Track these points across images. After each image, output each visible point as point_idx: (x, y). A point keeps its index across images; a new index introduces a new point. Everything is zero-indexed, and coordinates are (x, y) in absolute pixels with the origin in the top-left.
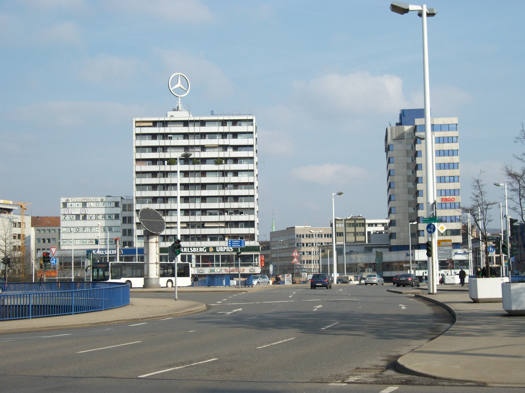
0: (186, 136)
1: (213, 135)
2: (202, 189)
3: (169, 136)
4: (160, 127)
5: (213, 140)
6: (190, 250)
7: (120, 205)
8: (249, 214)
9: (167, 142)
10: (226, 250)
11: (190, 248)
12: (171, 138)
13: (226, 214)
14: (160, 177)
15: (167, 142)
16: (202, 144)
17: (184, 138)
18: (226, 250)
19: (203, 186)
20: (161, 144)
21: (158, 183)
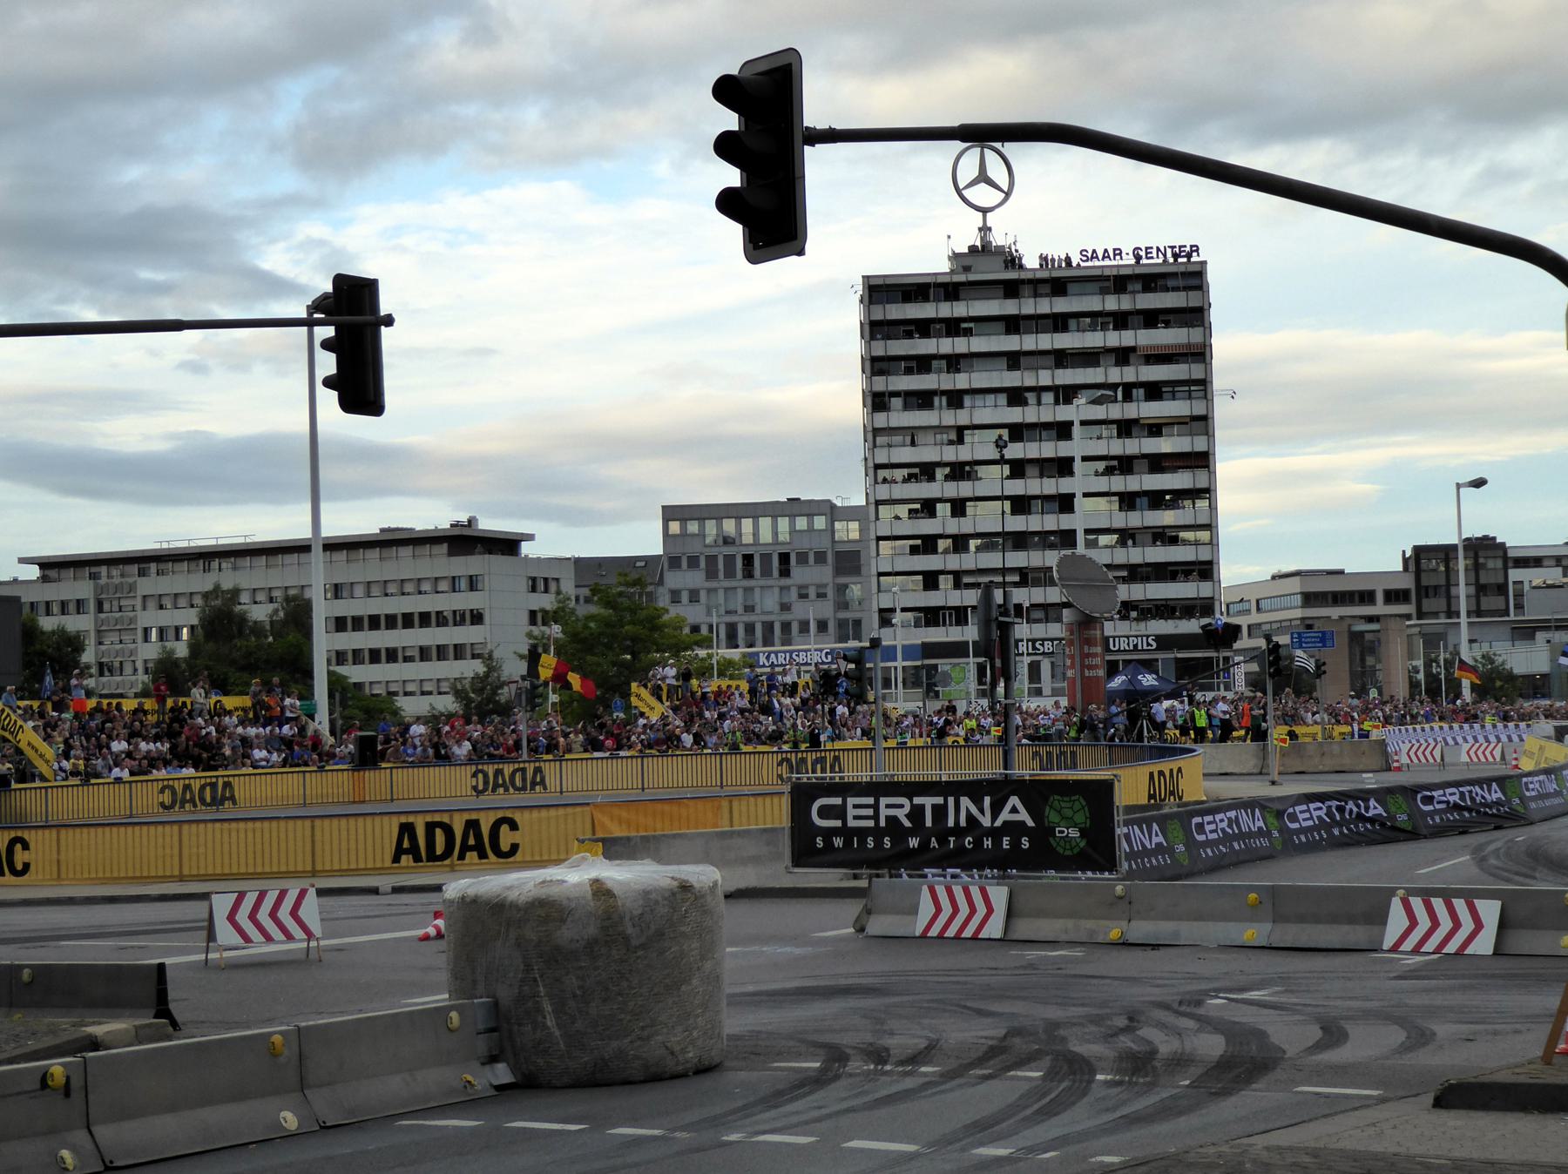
0: (1012, 324)
1: (1088, 358)
2: (1056, 330)
3: (964, 325)
4: (937, 300)
5: (1090, 370)
6: (1034, 648)
7: (831, 626)
8: (1191, 435)
9: (960, 345)
10: (1136, 646)
11: (1034, 641)
12: (968, 333)
13: (1130, 542)
14: (940, 371)
15: (960, 345)
16: (1057, 346)
17: (1008, 332)
18: (1136, 646)
19: (1059, 323)
20: (944, 387)
21: (934, 386)
